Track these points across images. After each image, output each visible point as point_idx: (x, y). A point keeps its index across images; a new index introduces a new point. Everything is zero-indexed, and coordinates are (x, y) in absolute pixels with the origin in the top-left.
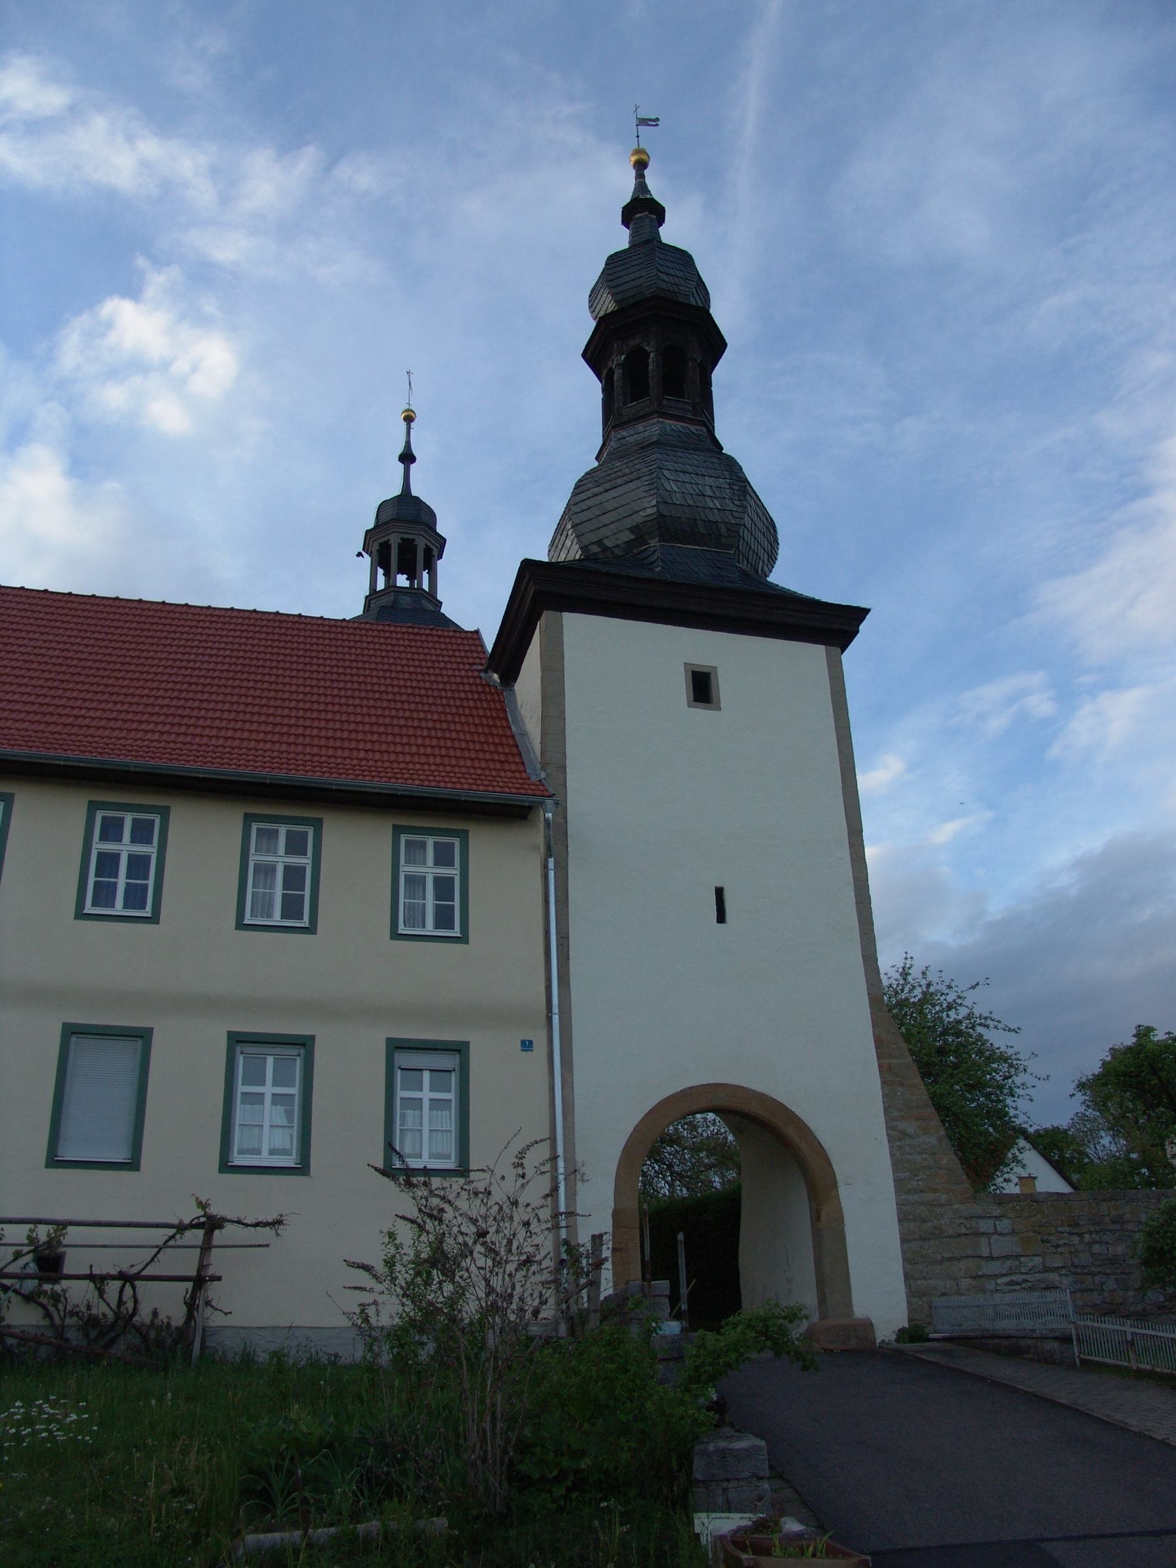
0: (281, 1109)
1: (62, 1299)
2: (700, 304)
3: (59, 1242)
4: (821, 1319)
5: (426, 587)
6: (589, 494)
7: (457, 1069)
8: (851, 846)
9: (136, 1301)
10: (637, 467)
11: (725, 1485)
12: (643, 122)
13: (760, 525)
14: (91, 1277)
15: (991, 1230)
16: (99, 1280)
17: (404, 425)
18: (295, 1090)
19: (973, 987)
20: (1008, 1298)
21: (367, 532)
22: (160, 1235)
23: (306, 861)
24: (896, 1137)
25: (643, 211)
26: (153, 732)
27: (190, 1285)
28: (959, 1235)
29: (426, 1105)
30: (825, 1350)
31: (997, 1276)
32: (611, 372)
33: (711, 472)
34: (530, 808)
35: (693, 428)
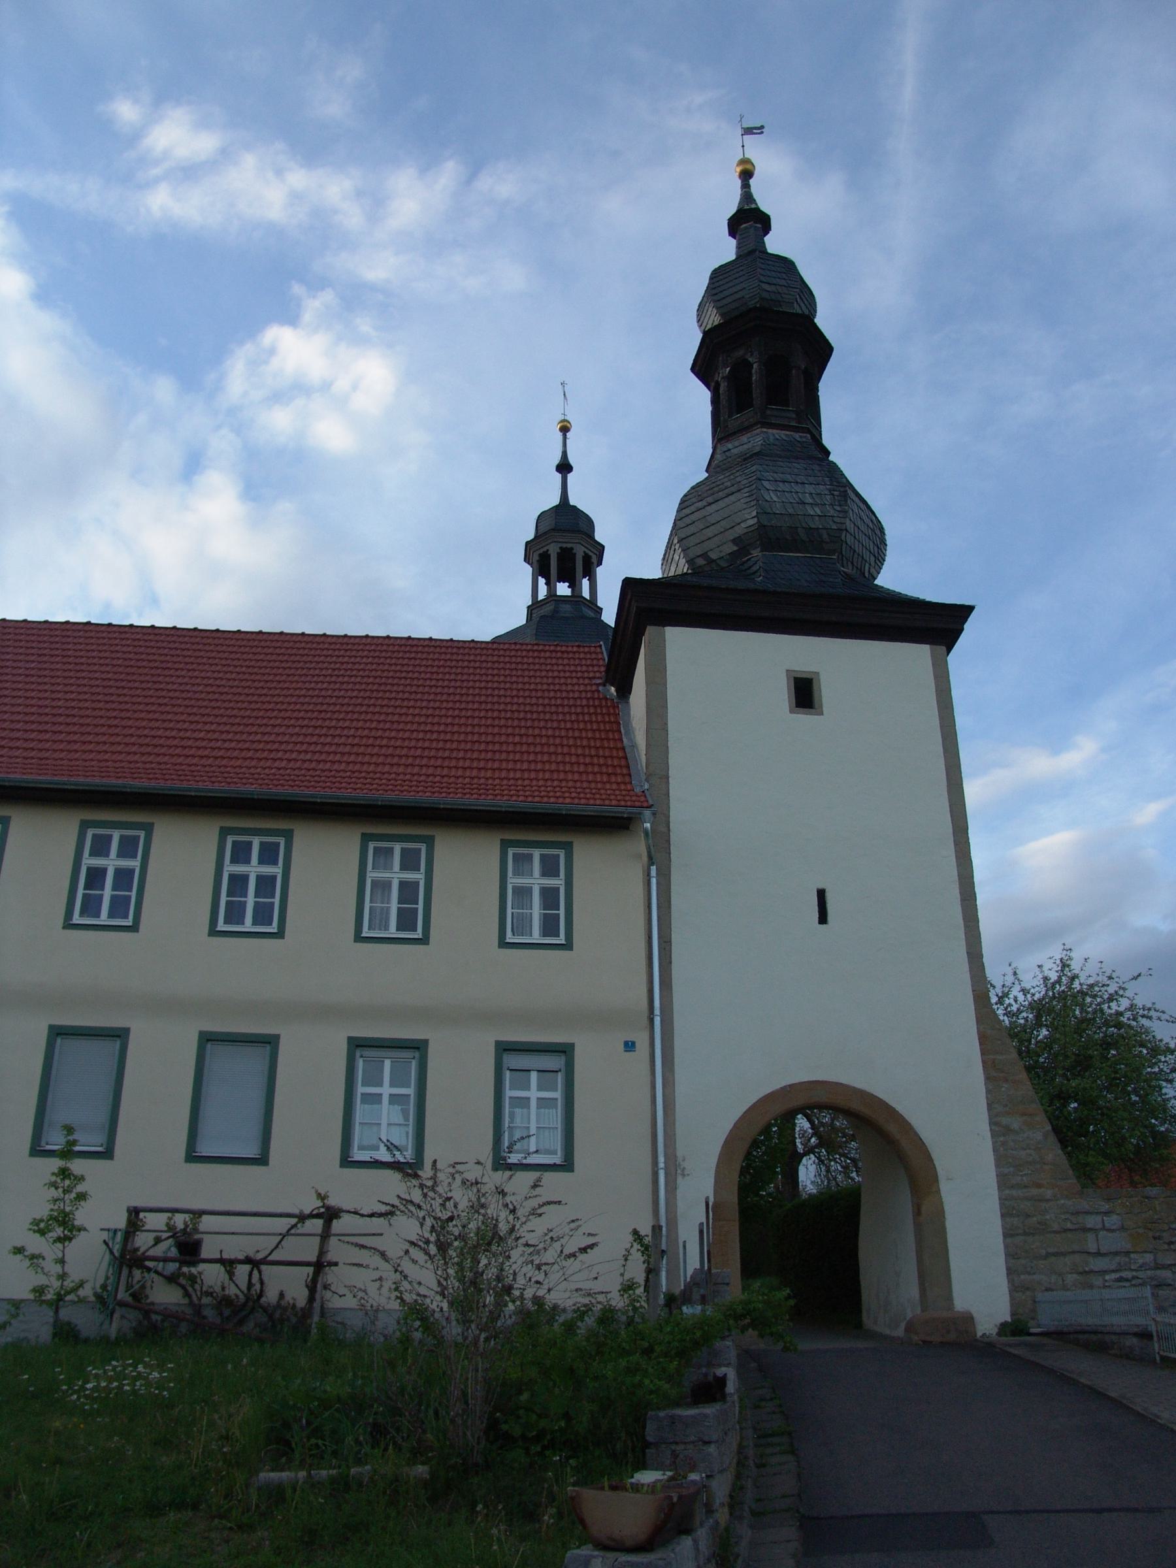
0: (398, 1108)
1: (199, 1281)
2: (807, 312)
3: (196, 1230)
4: (923, 1311)
5: (586, 593)
6: (693, 508)
7: (563, 1070)
8: (956, 844)
9: (262, 1283)
10: (738, 479)
11: (673, 1447)
12: (748, 131)
13: (863, 528)
14: (221, 1261)
15: (1100, 1226)
16: (229, 1264)
17: (560, 435)
18: (410, 1091)
19: (1135, 978)
20: (1122, 1293)
21: (527, 543)
22: (283, 1224)
23: (419, 876)
24: (999, 1131)
25: (749, 221)
26: (281, 759)
27: (311, 1270)
28: (1066, 1230)
29: (533, 1104)
30: (924, 1342)
31: (1105, 1272)
32: (718, 385)
33: (811, 479)
34: (630, 819)
35: (797, 436)
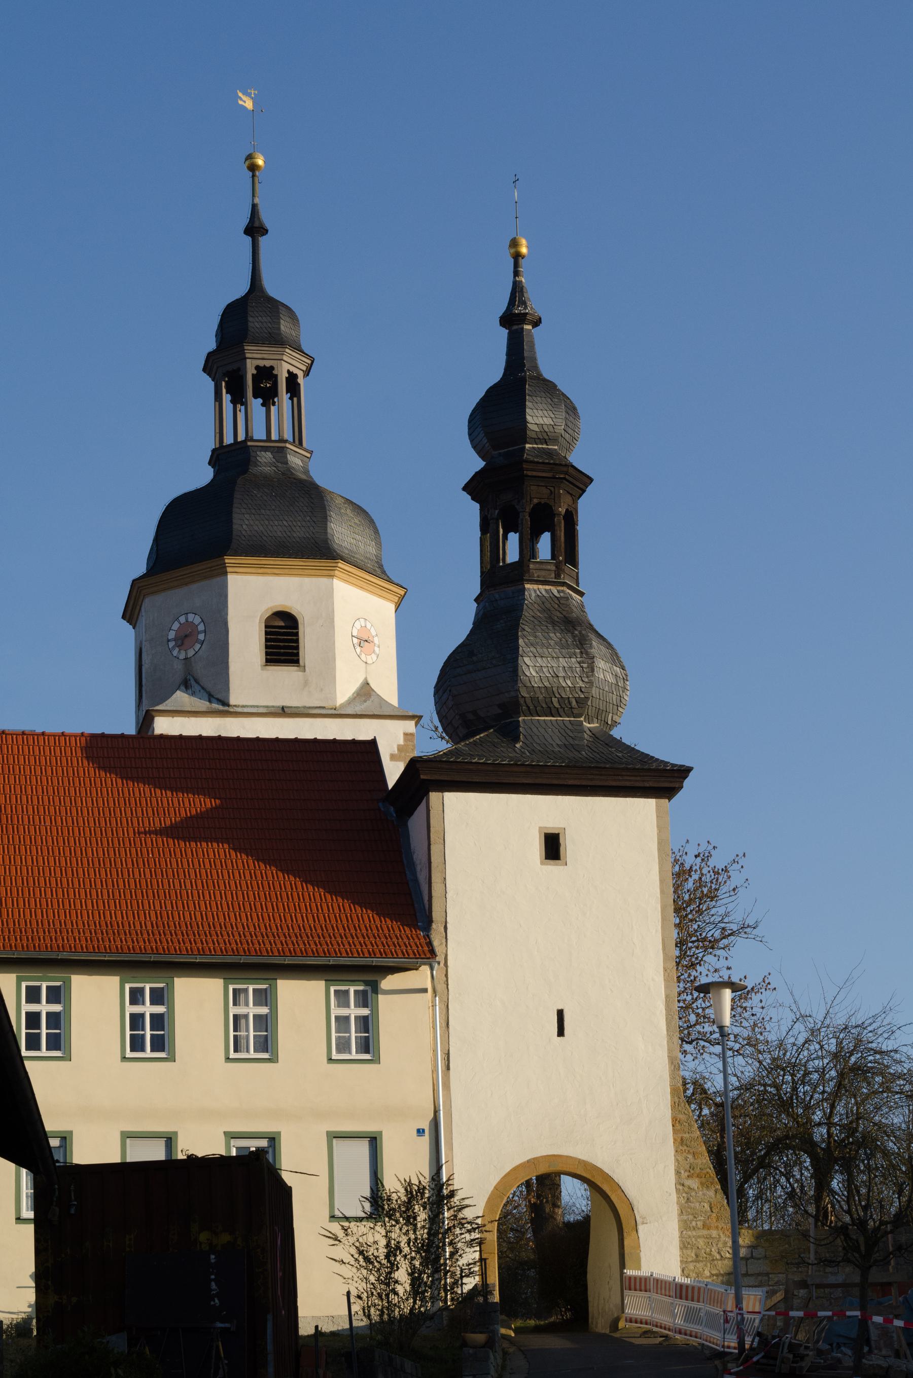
35: (554, 590)
